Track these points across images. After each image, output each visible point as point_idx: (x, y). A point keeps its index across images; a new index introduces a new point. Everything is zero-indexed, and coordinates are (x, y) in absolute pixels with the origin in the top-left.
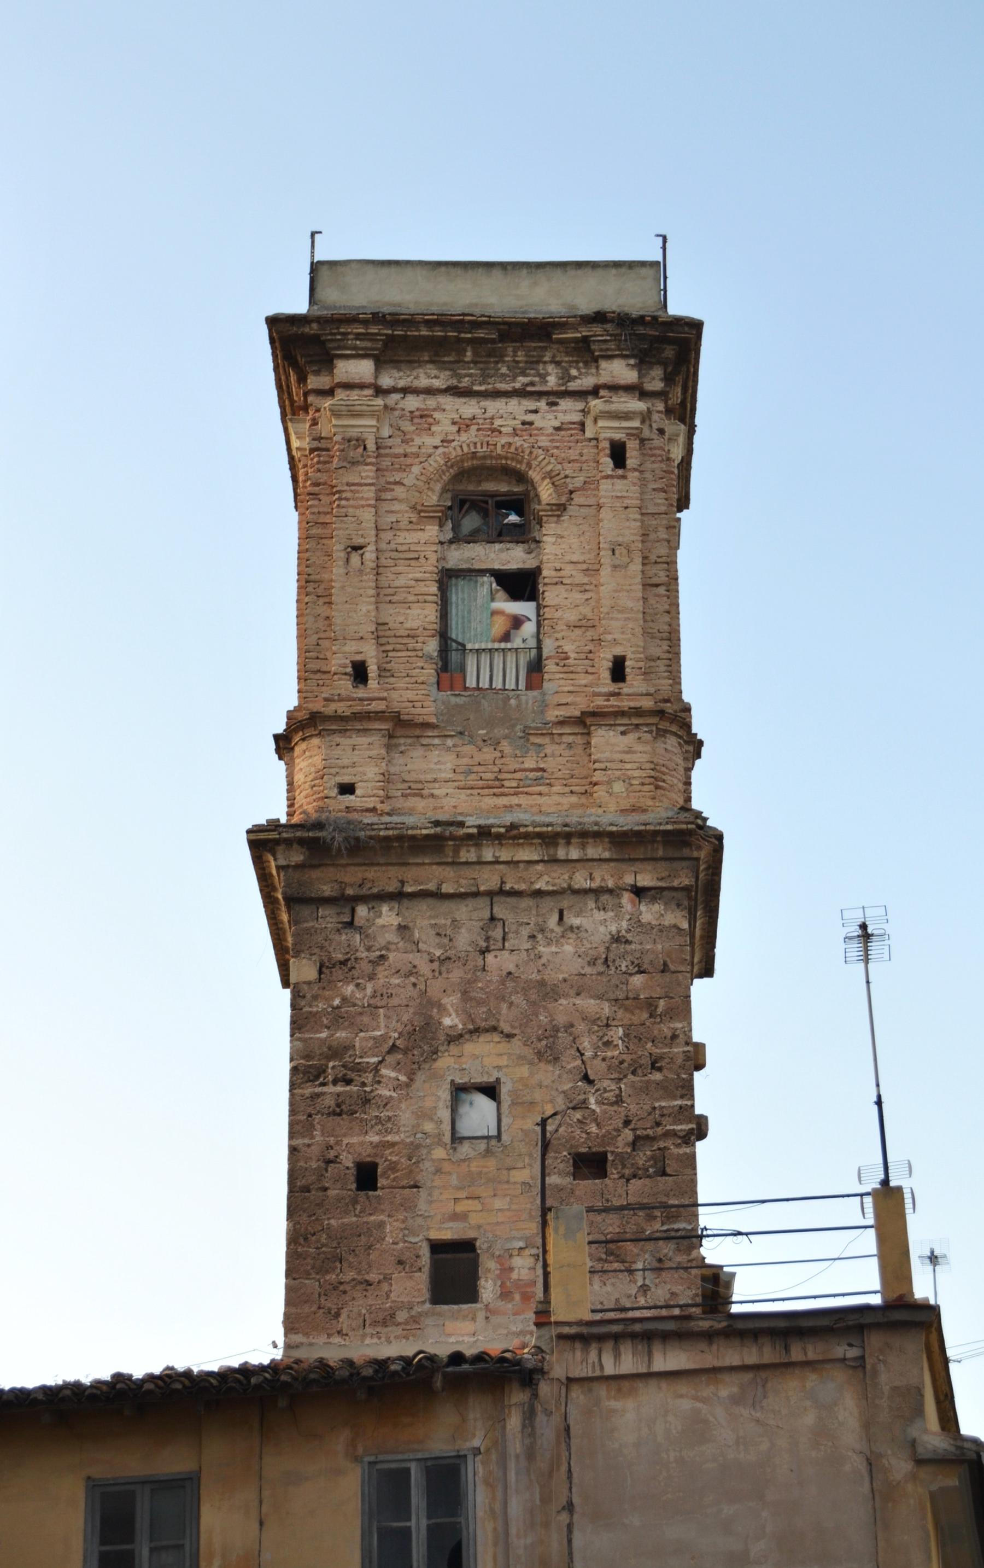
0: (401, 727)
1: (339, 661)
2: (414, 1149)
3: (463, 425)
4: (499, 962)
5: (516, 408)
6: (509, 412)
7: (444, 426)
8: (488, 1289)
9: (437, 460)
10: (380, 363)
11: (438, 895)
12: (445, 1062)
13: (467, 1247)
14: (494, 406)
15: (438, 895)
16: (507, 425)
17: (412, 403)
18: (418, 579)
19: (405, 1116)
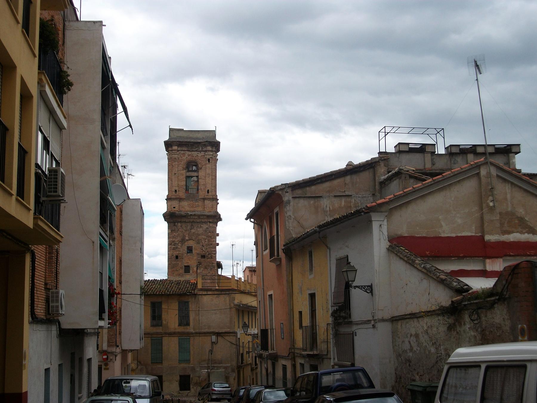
0: (180, 199)
1: (174, 190)
2: (182, 254)
3: (189, 155)
4: (193, 231)
5: (196, 153)
6: (195, 154)
7: (186, 156)
8: (191, 272)
9: (185, 161)
10: (178, 146)
11: (185, 222)
12: (186, 243)
13: (188, 266)
14: (193, 153)
15: (185, 222)
16: (195, 155)
17: (182, 152)
18: (183, 178)
19: (181, 250)
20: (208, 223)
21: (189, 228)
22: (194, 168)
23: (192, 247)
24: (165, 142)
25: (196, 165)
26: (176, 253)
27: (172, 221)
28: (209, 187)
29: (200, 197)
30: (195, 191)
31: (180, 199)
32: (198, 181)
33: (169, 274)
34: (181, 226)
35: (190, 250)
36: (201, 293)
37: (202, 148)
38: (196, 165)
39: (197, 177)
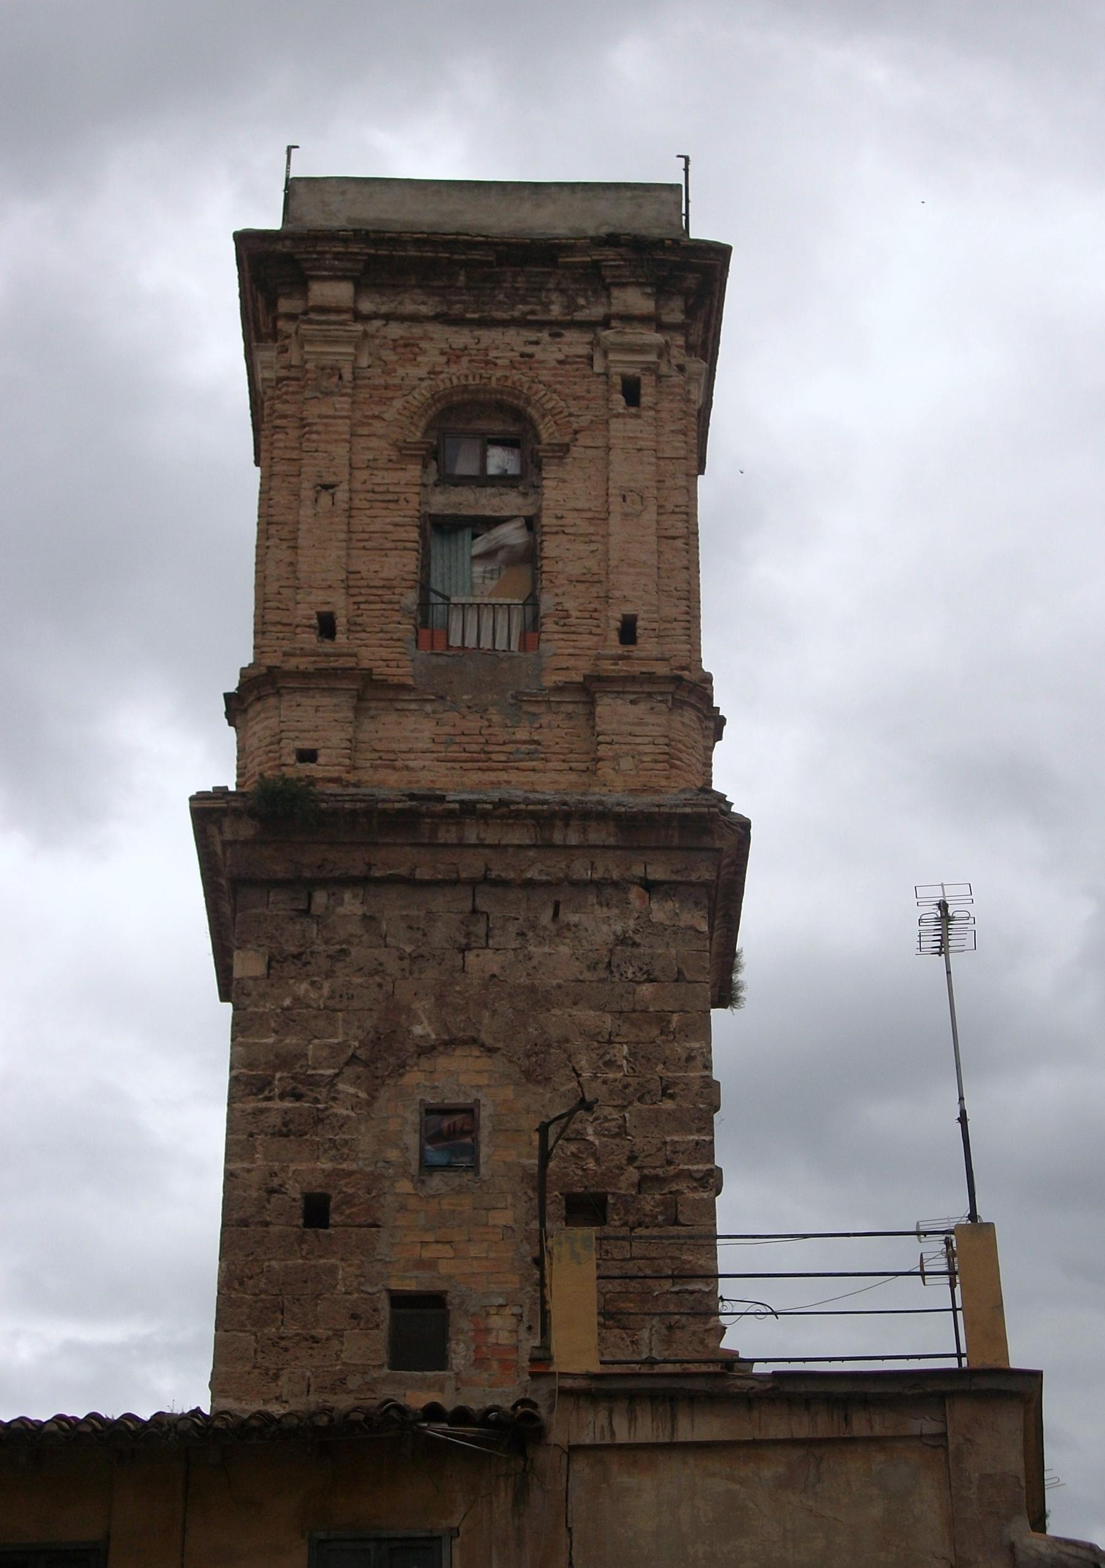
0: (369, 690)
1: (305, 611)
3: (453, 356)
4: (483, 962)
5: (515, 339)
7: (431, 356)
9: (423, 392)
10: (360, 288)
11: (410, 882)
12: (413, 1077)
14: (487, 336)
15: (410, 882)
16: (503, 357)
17: (396, 330)
20: (635, 894)
21: (441, 934)
22: (499, 460)
23: (470, 1111)
24: (198, 1408)
25: (519, 436)
26: (306, 1170)
27: (280, 870)
28: (634, 595)
29: (551, 679)
30: (501, 633)
31: (369, 690)
32: (530, 557)
33: (217, 1385)
34: (368, 920)
35: (451, 1133)
36: (589, 1426)
37: (571, 307)
38: (519, 436)
39: (531, 524)
